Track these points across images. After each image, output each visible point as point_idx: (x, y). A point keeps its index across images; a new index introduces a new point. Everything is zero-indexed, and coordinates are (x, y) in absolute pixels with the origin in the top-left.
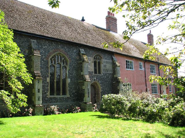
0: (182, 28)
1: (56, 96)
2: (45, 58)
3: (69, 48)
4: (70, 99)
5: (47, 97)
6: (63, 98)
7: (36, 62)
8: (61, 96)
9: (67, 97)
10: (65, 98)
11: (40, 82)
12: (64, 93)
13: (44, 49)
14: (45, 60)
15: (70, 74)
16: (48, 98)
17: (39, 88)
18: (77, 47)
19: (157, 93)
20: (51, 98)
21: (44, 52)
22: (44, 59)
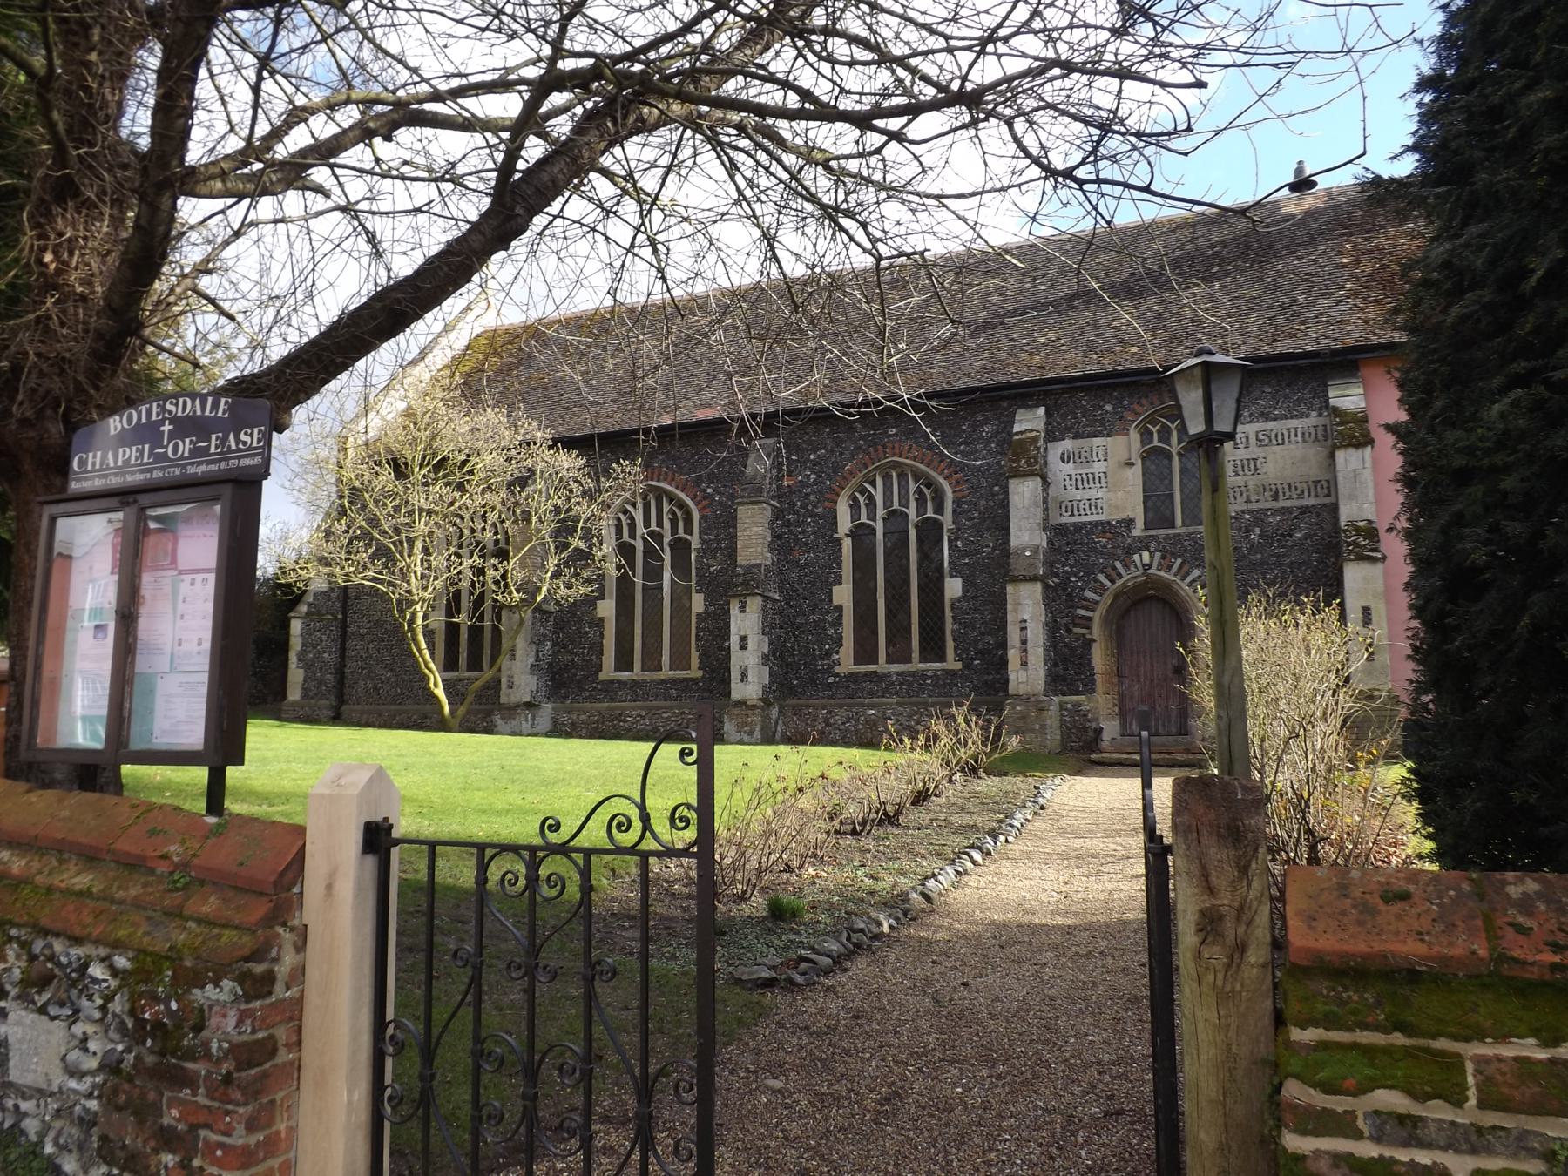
0: (423, 340)
1: (883, 666)
2: (819, 501)
3: (951, 427)
4: (963, 678)
5: (837, 669)
6: (922, 675)
7: (745, 530)
8: (916, 665)
9: (947, 672)
10: (930, 678)
11: (748, 609)
12: (932, 647)
13: (815, 463)
14: (820, 510)
15: (966, 554)
16: (837, 675)
17: (742, 633)
18: (1005, 405)
19: (1120, 576)
20: (852, 676)
21: (813, 476)
22: (815, 506)
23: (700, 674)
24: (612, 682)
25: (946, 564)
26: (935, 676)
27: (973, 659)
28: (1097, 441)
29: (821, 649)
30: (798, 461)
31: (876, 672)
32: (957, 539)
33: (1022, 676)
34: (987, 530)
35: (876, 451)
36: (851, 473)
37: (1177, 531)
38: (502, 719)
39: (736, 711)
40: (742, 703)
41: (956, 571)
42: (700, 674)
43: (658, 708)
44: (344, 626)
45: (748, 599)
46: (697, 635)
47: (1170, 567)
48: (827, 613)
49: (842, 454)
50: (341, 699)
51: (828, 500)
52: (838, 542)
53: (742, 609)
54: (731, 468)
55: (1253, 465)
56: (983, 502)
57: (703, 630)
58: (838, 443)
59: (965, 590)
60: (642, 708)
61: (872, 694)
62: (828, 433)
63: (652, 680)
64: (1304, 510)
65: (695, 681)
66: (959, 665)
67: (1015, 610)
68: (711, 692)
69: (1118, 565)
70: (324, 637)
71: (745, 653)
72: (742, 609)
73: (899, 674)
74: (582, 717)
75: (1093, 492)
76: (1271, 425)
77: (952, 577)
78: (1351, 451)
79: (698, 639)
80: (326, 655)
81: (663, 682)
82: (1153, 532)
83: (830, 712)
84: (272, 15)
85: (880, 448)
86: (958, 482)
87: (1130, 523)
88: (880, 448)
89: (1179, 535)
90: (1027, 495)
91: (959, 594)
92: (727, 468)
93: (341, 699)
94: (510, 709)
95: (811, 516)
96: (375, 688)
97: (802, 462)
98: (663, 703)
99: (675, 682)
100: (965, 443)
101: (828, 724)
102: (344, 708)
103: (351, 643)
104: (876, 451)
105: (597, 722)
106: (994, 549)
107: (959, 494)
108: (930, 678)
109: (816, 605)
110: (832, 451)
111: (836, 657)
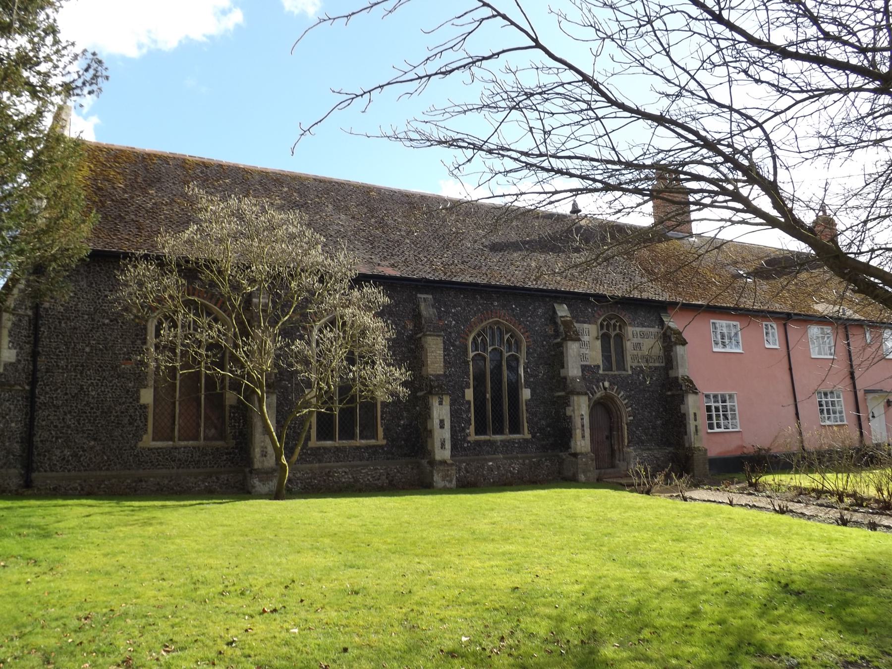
5: (469, 439)
7: (432, 352)
9: (525, 440)
11: (444, 403)
12: (515, 428)
13: (454, 314)
15: (532, 376)
16: (469, 442)
17: (441, 418)
18: (548, 300)
20: (477, 443)
21: (454, 322)
23: (384, 442)
24: (319, 448)
25: (523, 381)
26: (519, 443)
27: (536, 433)
28: (586, 326)
29: (459, 426)
30: (444, 312)
31: (490, 440)
32: (528, 367)
33: (583, 443)
34: (541, 364)
35: (487, 312)
36: (475, 324)
37: (613, 373)
38: (260, 481)
39: (441, 468)
40: (443, 462)
41: (527, 385)
42: (384, 442)
43: (357, 466)
44: (31, 398)
45: (444, 397)
46: (382, 416)
47: (613, 389)
48: (462, 404)
49: (469, 311)
50: (28, 466)
51: (463, 338)
52: (468, 362)
53: (441, 403)
54: (404, 309)
55: (638, 346)
56: (539, 349)
57: (386, 413)
58: (468, 305)
59: (532, 395)
60: (345, 467)
61: (488, 453)
62: (463, 298)
63: (350, 447)
64: (656, 368)
65: (382, 447)
66: (529, 436)
67: (578, 409)
68: (393, 454)
69: (594, 387)
70: (12, 407)
71: (444, 430)
72: (441, 403)
73: (501, 441)
74: (298, 475)
75: (584, 350)
76: (644, 329)
77: (525, 388)
78: (681, 346)
79: (382, 419)
80: (13, 425)
81: (358, 448)
82: (606, 373)
83: (468, 464)
84: (714, 9)
85: (489, 312)
86: (528, 337)
87: (598, 366)
88: (489, 312)
89: (615, 375)
90: (575, 350)
91: (529, 397)
92: (401, 309)
93: (28, 466)
94: (267, 473)
95: (453, 346)
96: (75, 455)
97: (447, 312)
98: (359, 463)
99: (367, 447)
100: (531, 316)
101: (468, 472)
102: (34, 475)
103: (41, 414)
104: (487, 312)
105: (311, 478)
106: (544, 374)
107: (529, 344)
108: (516, 443)
109: (456, 400)
110: (464, 309)
111: (468, 431)
